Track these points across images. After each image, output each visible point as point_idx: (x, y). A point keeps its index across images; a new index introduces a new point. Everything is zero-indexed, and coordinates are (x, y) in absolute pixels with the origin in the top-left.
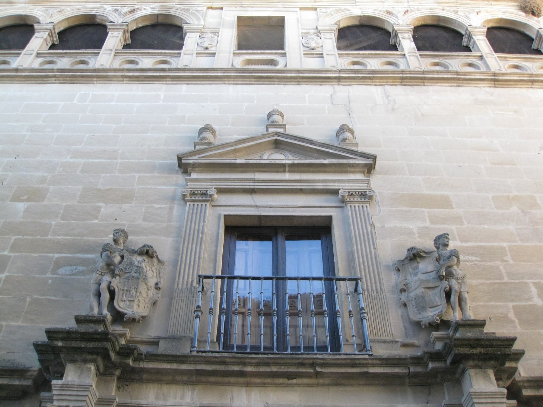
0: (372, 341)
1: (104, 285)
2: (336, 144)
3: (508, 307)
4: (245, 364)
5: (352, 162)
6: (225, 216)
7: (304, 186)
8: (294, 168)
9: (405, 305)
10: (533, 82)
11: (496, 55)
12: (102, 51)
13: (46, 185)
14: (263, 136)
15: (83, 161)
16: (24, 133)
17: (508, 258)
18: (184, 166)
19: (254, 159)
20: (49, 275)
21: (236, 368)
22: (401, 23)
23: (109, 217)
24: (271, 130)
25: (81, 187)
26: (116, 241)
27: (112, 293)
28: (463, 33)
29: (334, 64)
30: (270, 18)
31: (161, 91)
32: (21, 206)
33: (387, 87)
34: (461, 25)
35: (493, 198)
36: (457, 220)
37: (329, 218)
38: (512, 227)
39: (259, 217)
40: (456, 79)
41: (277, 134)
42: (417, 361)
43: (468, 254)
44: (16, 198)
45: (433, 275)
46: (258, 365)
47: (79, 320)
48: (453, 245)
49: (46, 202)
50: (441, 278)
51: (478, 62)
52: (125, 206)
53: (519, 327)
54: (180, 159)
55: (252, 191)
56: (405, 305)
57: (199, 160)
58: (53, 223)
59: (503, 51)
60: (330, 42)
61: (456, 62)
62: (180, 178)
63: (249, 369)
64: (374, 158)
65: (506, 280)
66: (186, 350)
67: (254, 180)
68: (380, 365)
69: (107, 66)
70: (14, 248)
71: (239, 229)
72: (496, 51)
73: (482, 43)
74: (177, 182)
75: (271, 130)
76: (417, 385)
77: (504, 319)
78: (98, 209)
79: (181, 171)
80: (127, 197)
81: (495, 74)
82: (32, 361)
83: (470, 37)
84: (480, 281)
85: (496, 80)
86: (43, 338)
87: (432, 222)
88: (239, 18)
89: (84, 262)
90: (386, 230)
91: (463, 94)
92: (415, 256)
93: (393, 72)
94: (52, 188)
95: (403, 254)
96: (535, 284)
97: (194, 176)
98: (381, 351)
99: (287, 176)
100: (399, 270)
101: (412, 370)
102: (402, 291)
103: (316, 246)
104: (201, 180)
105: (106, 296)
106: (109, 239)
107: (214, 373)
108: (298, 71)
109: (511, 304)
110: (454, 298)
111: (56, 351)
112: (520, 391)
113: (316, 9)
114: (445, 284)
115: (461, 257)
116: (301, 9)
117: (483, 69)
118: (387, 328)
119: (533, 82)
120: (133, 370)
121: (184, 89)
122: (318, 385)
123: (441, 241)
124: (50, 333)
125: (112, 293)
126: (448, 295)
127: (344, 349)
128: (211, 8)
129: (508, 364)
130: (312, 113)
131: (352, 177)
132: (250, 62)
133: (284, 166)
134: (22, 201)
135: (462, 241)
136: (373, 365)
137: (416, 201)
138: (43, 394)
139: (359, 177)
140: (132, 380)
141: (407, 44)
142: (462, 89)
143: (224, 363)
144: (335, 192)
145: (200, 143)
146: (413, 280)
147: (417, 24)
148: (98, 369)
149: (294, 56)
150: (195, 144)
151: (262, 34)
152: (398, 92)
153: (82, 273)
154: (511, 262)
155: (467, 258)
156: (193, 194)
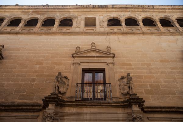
0: (113, 97)
1: (56, 86)
2: (106, 51)
3: (143, 90)
4: (86, 103)
5: (110, 55)
6: (82, 68)
7: (99, 61)
8: (97, 57)
9: (120, 89)
10: (152, 34)
11: (144, 27)
12: (54, 27)
13: (43, 61)
14: (90, 49)
15: (51, 55)
16: (37, 48)
17: (143, 78)
18: (73, 56)
19: (89, 55)
20: (44, 83)
21: (84, 104)
22: (122, 19)
23: (61, 68)
24: (92, 48)
25: (51, 62)
26: (59, 75)
27: (58, 87)
28: (171, 21)
29: (107, 30)
30: (92, 18)
31: (67, 37)
32: (38, 66)
33: (119, 36)
34: (137, 19)
35: (141, 63)
36: (133, 69)
37: (105, 69)
38: (145, 71)
39: (90, 68)
40: (134, 34)
41: (93, 49)
42: (122, 102)
43: (135, 77)
44: (36, 65)
45: (126, 83)
46: (89, 103)
47: (51, 94)
48: (131, 75)
49: (43, 65)
50: (128, 84)
51: (140, 29)
52: (60, 66)
53: (145, 94)
54: (72, 55)
55: (88, 62)
56: (120, 89)
57: (77, 54)
58: (45, 70)
59: (146, 26)
60: (106, 24)
61: (134, 29)
62: (73, 59)
63: (87, 104)
64: (115, 55)
65: (143, 83)
66: (74, 100)
67: (89, 60)
68: (114, 103)
69: (55, 31)
70: (37, 76)
71: (85, 71)
72: (144, 26)
73: (141, 23)
74: (72, 60)
75: (92, 48)
76: (122, 107)
77: (142, 93)
78: (55, 67)
79: (72, 57)
80: (60, 64)
81: (143, 32)
82: (41, 102)
83: (138, 22)
84: (137, 84)
85: (143, 33)
86: (44, 98)
87: (127, 69)
88: (85, 18)
89: (52, 80)
90: (114, 74)
91: (136, 37)
92: (123, 78)
93: (120, 32)
94: (44, 62)
95: (120, 78)
96: (149, 84)
97: (75, 59)
98: (114, 100)
99: (96, 59)
100: (119, 81)
101: (121, 104)
102: (120, 86)
103: (102, 74)
104: (77, 60)
105: (57, 88)
106: (57, 74)
107: (80, 105)
108: (98, 32)
109: (143, 89)
110: (130, 88)
111: (47, 101)
112: (144, 109)
113: (103, 15)
114: (129, 85)
115: (133, 78)
116: (99, 15)
117: (141, 31)
118: (117, 93)
119: (152, 34)
120: (63, 105)
121: (73, 37)
122: (102, 107)
123: (128, 74)
124: (45, 97)
125: (58, 87)
126: (129, 87)
127: (107, 99)
128: (79, 15)
129: (141, 104)
130: (101, 42)
131: (110, 59)
132: (87, 29)
133: (95, 56)
134: (38, 65)
135: (133, 74)
136: (113, 103)
137: (124, 64)
138: (44, 110)
139: (111, 59)
140: (63, 107)
141: (124, 24)
142: (136, 36)
143: (82, 103)
144: (106, 62)
145: (77, 51)
146: (122, 84)
147: (126, 18)
148: (55, 104)
149: (98, 28)
150: (76, 51)
151: (90, 23)
152: (121, 37)
153: (52, 82)
154: (144, 79)
155: (134, 78)
156: (75, 63)
